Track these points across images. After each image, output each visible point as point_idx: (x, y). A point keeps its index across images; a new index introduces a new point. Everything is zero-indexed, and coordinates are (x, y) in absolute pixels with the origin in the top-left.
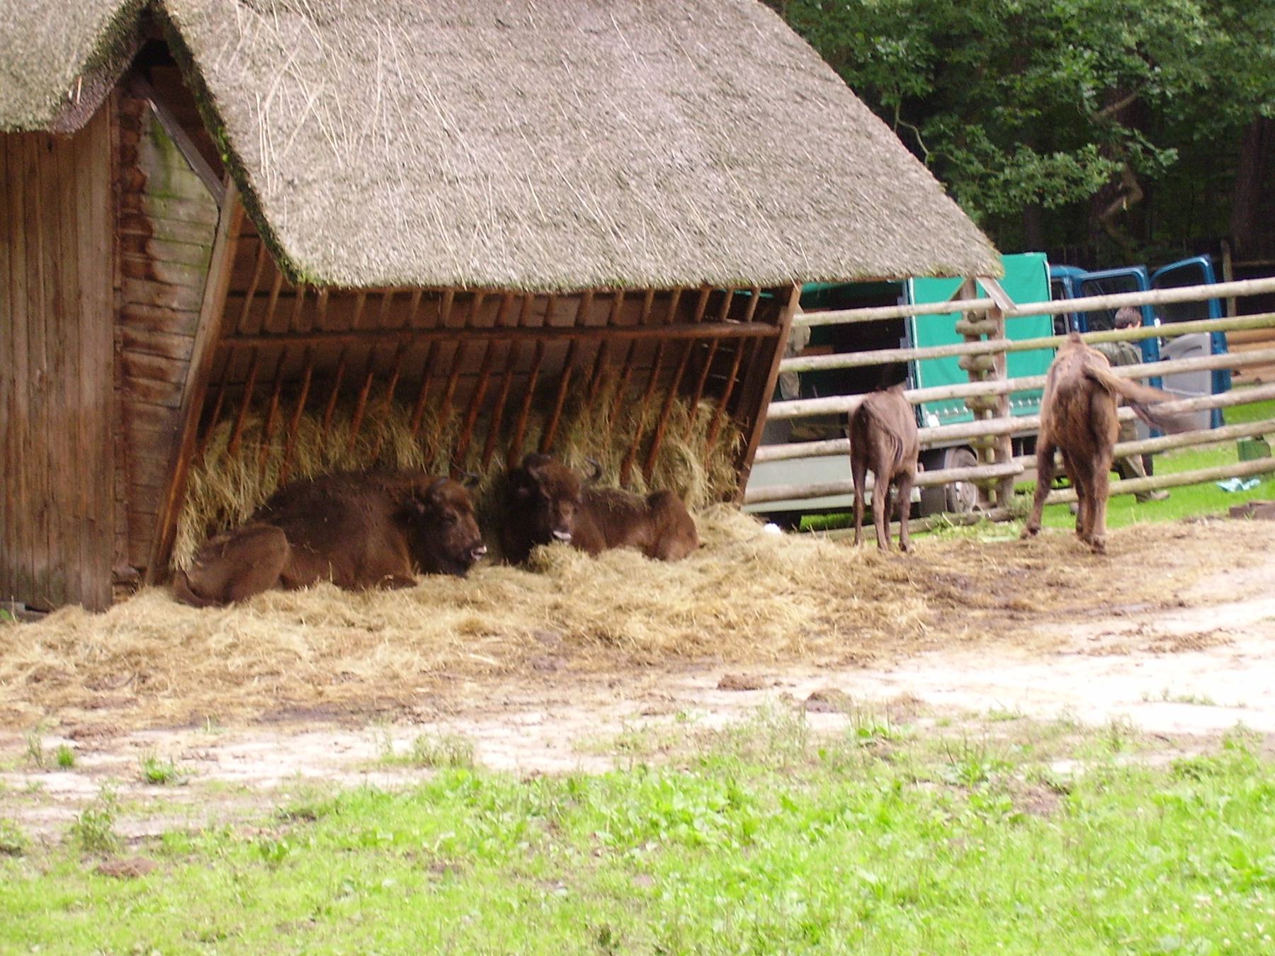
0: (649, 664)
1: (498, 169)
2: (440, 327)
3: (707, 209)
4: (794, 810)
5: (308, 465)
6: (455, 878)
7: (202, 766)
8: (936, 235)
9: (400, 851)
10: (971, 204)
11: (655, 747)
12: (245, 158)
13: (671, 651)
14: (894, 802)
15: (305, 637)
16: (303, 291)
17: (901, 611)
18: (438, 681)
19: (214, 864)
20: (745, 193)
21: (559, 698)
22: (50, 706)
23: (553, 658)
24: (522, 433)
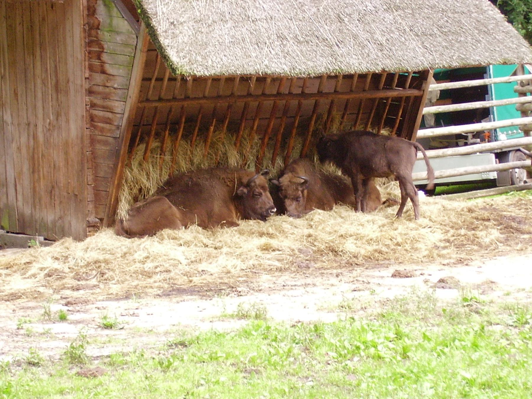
0: (356, 264)
1: (277, 14)
2: (249, 95)
3: (385, 32)
4: (429, 340)
5: (184, 166)
6: (256, 376)
7: (130, 319)
8: (502, 43)
9: (228, 364)
10: (520, 26)
11: (359, 308)
12: (149, 11)
13: (368, 258)
14: (480, 336)
15: (183, 252)
16: (179, 78)
17: (486, 236)
18: (250, 274)
19: (136, 370)
20: (404, 23)
21: (311, 283)
22: (55, 289)
23: (308, 262)
24: (291, 147)
